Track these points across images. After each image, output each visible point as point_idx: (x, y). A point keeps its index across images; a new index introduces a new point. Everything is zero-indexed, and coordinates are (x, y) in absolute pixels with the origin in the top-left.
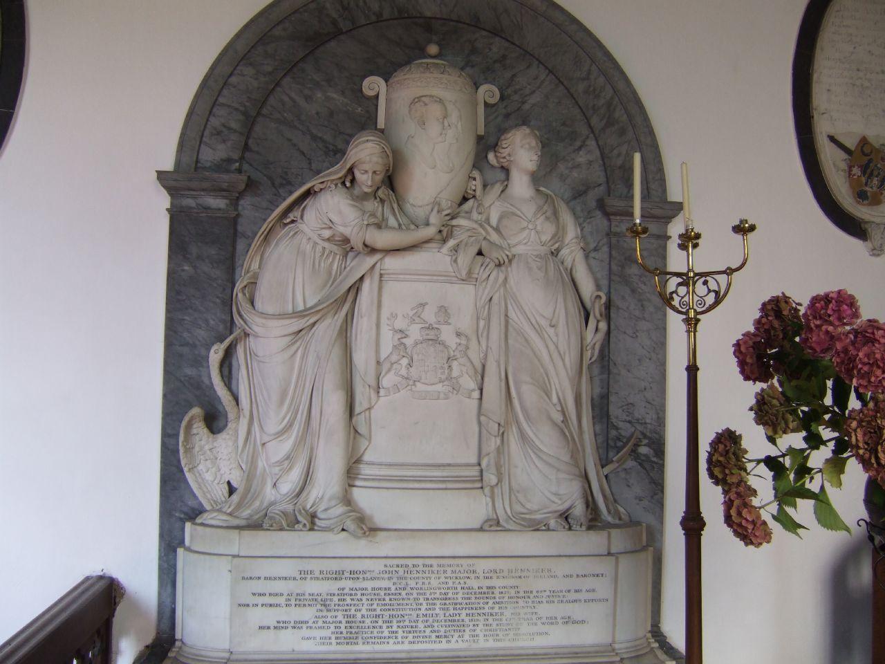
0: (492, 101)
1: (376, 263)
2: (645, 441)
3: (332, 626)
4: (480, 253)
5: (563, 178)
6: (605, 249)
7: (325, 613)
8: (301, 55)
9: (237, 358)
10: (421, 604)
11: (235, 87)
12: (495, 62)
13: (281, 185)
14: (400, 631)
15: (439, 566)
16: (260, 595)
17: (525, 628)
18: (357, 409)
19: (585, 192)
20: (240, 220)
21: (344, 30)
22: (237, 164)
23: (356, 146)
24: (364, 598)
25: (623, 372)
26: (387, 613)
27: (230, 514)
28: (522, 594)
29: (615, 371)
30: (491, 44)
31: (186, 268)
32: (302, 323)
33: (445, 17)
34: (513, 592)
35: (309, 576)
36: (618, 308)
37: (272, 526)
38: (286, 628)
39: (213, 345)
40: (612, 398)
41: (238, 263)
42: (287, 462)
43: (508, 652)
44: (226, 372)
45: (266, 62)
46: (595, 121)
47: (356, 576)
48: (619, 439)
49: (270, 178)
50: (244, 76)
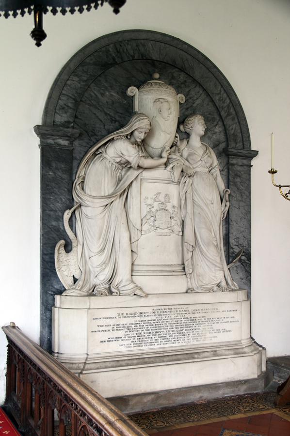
0: (182, 102)
3: (132, 338)
6: (226, 170)
7: (129, 333)
10: (168, 326)
11: (69, 86)
12: (182, 83)
13: (92, 135)
14: (159, 339)
15: (174, 309)
16: (101, 326)
17: (208, 335)
19: (218, 145)
21: (118, 63)
22: (72, 124)
24: (145, 325)
26: (154, 331)
27: (80, 290)
28: (207, 320)
29: (232, 223)
30: (180, 75)
31: (50, 173)
33: (161, 60)
35: (122, 316)
36: (232, 196)
37: (102, 294)
42: (104, 265)
45: (83, 75)
47: (141, 315)
50: (73, 81)
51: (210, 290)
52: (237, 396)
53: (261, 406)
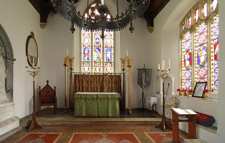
17: (3, 118)
46: (5, 44)
51: (3, 103)
52: (14, 133)
53: (25, 133)
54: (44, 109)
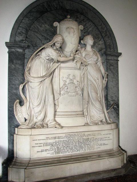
0: (82, 29)
1: (58, 66)
2: (115, 105)
4: (82, 63)
5: (97, 47)
8: (39, 16)
9: (26, 88)
13: (35, 46)
14: (69, 150)
18: (55, 99)
19: (102, 50)
20: (25, 55)
23: (57, 37)
24: (61, 143)
25: (110, 89)
26: (66, 146)
27: (27, 125)
28: (95, 139)
31: (13, 66)
32: (43, 79)
34: (93, 139)
35: (48, 139)
38: (43, 151)
39: (20, 85)
40: (109, 95)
41: (25, 65)
43: (92, 152)
44: (23, 91)
46: (103, 34)
48: (110, 104)
49: (32, 45)
54: (81, 175)
